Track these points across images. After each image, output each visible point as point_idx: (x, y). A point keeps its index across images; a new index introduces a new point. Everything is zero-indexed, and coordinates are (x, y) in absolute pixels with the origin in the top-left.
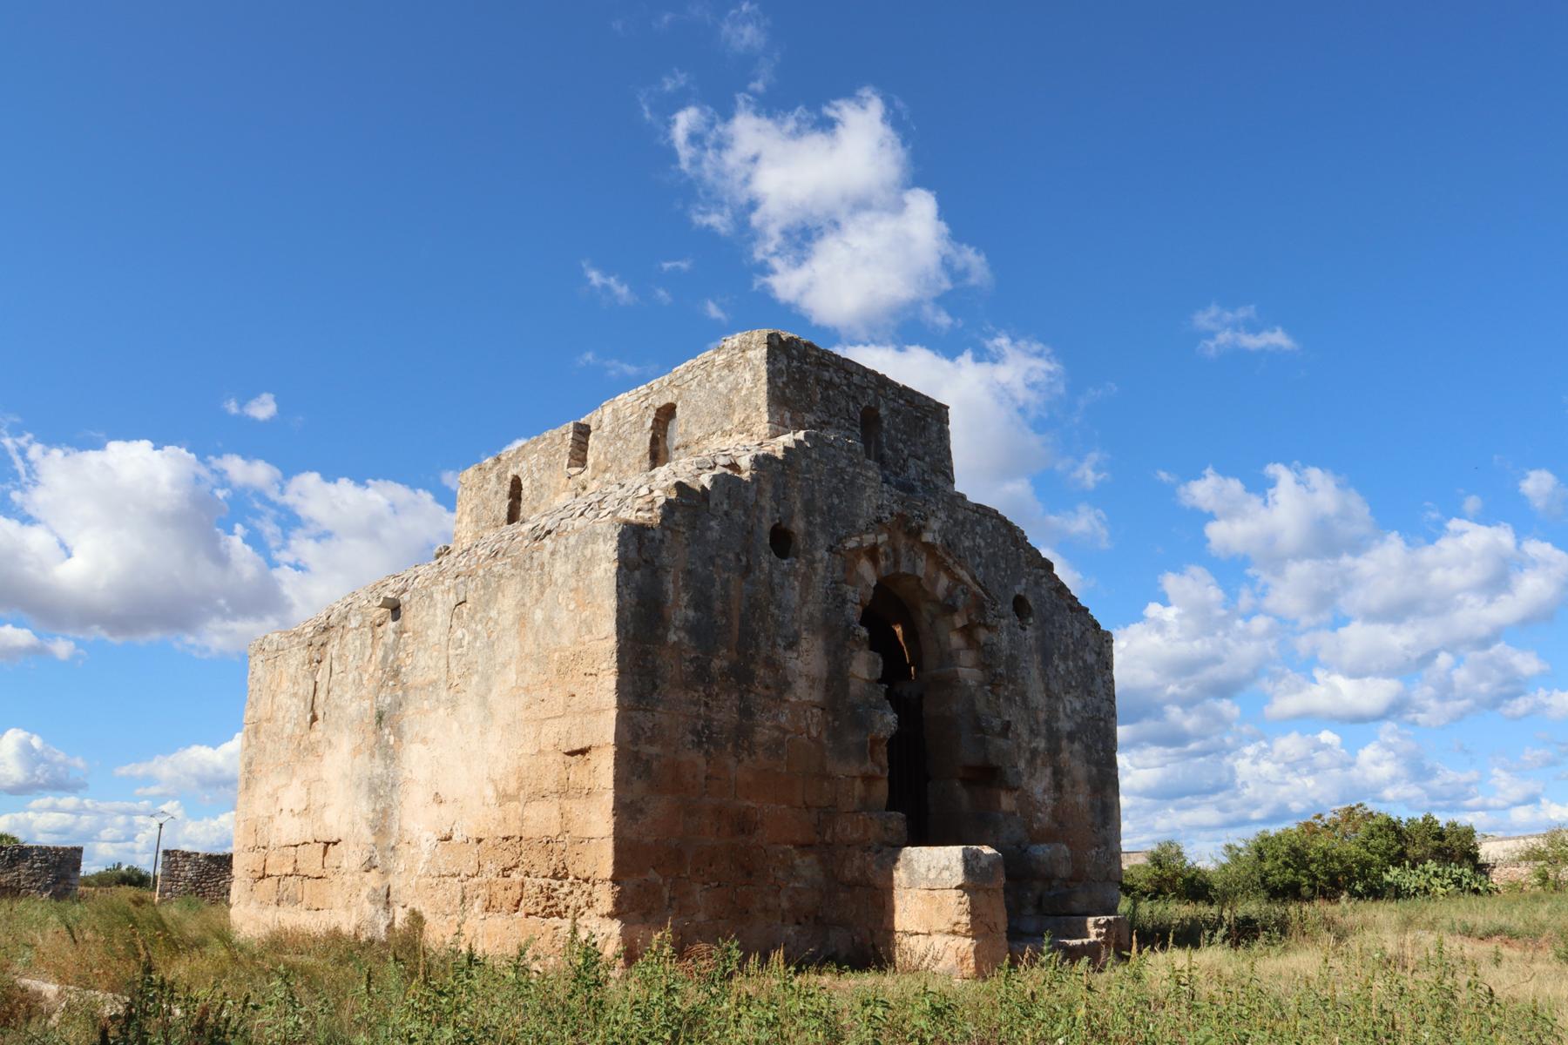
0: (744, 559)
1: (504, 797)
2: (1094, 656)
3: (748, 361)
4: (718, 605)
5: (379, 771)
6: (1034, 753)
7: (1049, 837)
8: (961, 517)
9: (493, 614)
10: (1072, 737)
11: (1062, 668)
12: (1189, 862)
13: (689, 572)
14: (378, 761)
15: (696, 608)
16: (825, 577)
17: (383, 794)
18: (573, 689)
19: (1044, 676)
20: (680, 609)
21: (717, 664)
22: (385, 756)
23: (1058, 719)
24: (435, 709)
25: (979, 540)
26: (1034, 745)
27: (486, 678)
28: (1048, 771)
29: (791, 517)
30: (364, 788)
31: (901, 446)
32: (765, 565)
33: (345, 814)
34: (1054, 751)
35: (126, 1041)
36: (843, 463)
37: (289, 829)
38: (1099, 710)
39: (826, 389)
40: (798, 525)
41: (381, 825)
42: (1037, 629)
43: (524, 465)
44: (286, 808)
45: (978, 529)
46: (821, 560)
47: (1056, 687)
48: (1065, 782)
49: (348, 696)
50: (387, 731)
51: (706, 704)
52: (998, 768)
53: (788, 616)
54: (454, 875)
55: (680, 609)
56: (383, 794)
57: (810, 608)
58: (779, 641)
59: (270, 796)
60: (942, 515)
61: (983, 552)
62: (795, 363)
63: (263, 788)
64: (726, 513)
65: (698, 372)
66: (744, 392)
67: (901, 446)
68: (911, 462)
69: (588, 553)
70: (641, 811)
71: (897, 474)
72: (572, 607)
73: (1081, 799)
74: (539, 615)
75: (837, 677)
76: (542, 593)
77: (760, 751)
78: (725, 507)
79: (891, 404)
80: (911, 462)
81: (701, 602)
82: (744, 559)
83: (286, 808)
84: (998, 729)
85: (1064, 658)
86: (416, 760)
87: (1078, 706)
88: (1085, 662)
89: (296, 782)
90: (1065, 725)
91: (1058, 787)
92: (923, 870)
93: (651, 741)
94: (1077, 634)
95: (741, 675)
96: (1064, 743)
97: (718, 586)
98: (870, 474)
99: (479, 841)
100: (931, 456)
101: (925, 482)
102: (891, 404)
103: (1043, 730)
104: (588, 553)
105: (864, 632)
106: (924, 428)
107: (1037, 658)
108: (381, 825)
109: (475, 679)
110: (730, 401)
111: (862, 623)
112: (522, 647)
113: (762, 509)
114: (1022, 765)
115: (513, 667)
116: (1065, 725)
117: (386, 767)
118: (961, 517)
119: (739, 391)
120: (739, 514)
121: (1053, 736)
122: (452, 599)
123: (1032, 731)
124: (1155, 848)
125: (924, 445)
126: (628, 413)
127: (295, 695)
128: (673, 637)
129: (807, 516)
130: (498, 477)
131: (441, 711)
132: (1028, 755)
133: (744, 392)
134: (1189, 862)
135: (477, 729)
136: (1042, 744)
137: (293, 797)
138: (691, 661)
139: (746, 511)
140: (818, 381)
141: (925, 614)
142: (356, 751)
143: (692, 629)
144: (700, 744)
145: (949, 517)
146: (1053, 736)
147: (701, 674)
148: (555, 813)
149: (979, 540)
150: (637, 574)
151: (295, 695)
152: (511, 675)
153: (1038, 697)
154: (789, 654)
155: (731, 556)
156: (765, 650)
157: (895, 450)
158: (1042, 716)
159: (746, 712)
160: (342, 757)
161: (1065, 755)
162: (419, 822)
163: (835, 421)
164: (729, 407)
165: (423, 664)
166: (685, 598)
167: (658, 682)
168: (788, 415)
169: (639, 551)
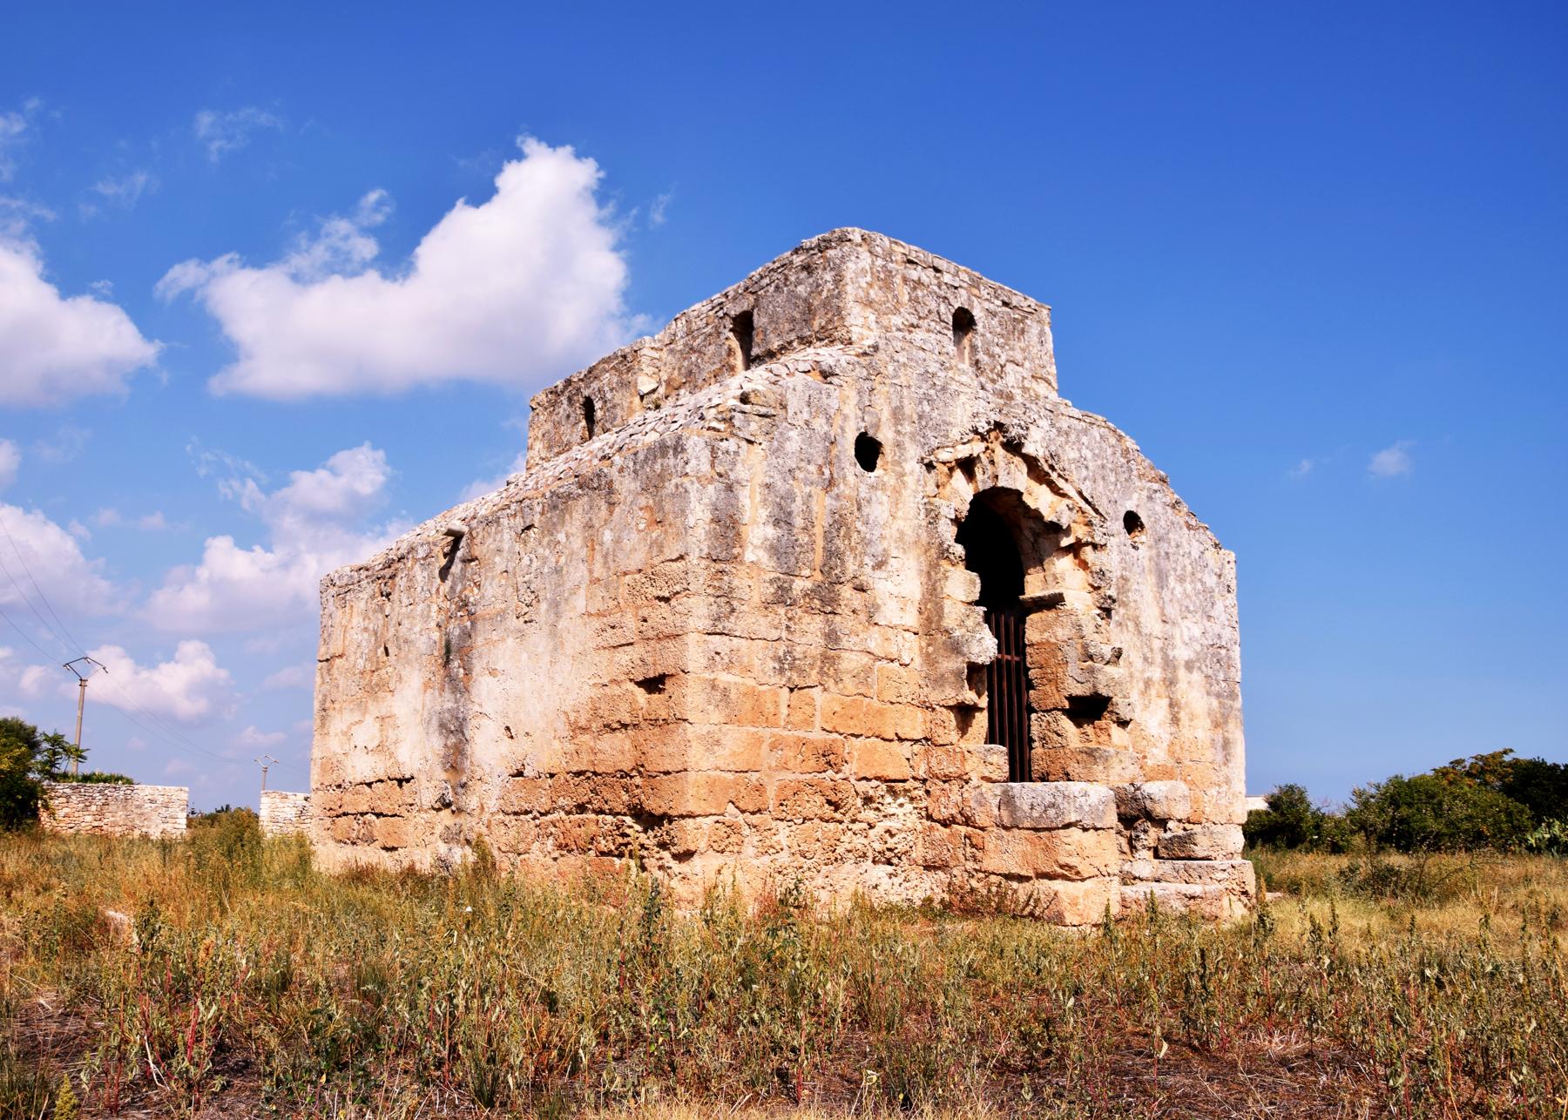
0: (827, 472)
1: (578, 729)
2: (1215, 578)
3: (828, 260)
4: (799, 522)
5: (449, 705)
6: (1148, 683)
7: (1164, 773)
8: (1065, 426)
9: (561, 537)
10: (1189, 666)
11: (1179, 590)
12: (1313, 807)
13: (768, 486)
14: (447, 694)
15: (777, 523)
16: (916, 491)
17: (455, 730)
18: (644, 612)
19: (1160, 599)
20: (758, 532)
21: (799, 585)
22: (455, 689)
23: (1174, 647)
24: (503, 640)
25: (1085, 452)
26: (1147, 675)
27: (555, 605)
28: (1166, 702)
29: (877, 426)
30: (435, 723)
31: (997, 350)
32: (851, 479)
33: (417, 751)
34: (1171, 683)
35: (1426, 1117)
36: (934, 367)
37: (362, 767)
38: (1219, 637)
39: (915, 289)
40: (885, 436)
41: (455, 759)
42: (1150, 547)
43: (595, 385)
44: (361, 745)
45: (1084, 439)
46: (912, 473)
47: (1172, 611)
48: (1182, 715)
49: (417, 629)
50: (456, 664)
51: (788, 627)
52: (1109, 699)
53: (877, 533)
54: (527, 812)
55: (758, 532)
56: (455, 730)
57: (900, 524)
58: (867, 560)
59: (345, 734)
60: (1044, 423)
61: (1091, 465)
62: (880, 262)
63: (338, 724)
64: (807, 423)
65: (776, 276)
66: (825, 294)
67: (997, 350)
68: (1010, 367)
69: (658, 467)
70: (718, 742)
71: (993, 381)
72: (642, 526)
73: (1200, 734)
74: (608, 536)
75: (933, 596)
76: (611, 513)
77: (847, 678)
78: (806, 416)
79: (987, 305)
80: (1010, 367)
81: (782, 519)
82: (827, 472)
83: (361, 745)
84: (1108, 656)
85: (1181, 580)
86: (486, 691)
87: (1197, 632)
88: (1203, 584)
89: (369, 719)
90: (1182, 654)
91: (1175, 720)
92: (1026, 808)
93: (728, 668)
94: (1195, 554)
95: (825, 599)
96: (1182, 673)
97: (799, 500)
98: (964, 379)
99: (552, 776)
100: (1032, 361)
101: (1025, 389)
102: (987, 305)
103: (1158, 658)
104: (658, 467)
105: (959, 550)
106: (1023, 331)
107: (1152, 579)
108: (455, 759)
109: (544, 606)
110: (810, 305)
111: (957, 540)
112: (591, 572)
113: (846, 417)
114: (1135, 697)
115: (582, 592)
116: (1182, 654)
117: (456, 701)
118: (1065, 426)
119: (820, 294)
120: (820, 424)
121: (1168, 664)
122: (519, 523)
123: (1146, 659)
124: (1276, 791)
125: (1023, 350)
126: (701, 324)
127: (366, 629)
128: (749, 556)
129: (896, 425)
130: (570, 399)
131: (510, 641)
132: (1141, 685)
133: (825, 294)
134: (1313, 807)
135: (547, 658)
136: (1156, 673)
137: (367, 733)
138: (771, 582)
139: (829, 419)
140: (905, 280)
141: (1027, 533)
142: (427, 685)
143: (775, 550)
144: (782, 671)
145: (1052, 425)
146: (1168, 664)
147: (782, 596)
148: (628, 745)
149: (1085, 452)
150: (711, 488)
151: (366, 629)
152: (580, 602)
153: (1151, 622)
154: (878, 573)
155: (812, 468)
156: (851, 567)
157: (992, 356)
158: (1157, 644)
159: (832, 637)
160: (413, 697)
161: (1182, 686)
162: (489, 751)
163: (924, 323)
164: (810, 311)
165: (491, 592)
166: (763, 513)
167: (735, 603)
168: (872, 318)
169: (713, 465)
